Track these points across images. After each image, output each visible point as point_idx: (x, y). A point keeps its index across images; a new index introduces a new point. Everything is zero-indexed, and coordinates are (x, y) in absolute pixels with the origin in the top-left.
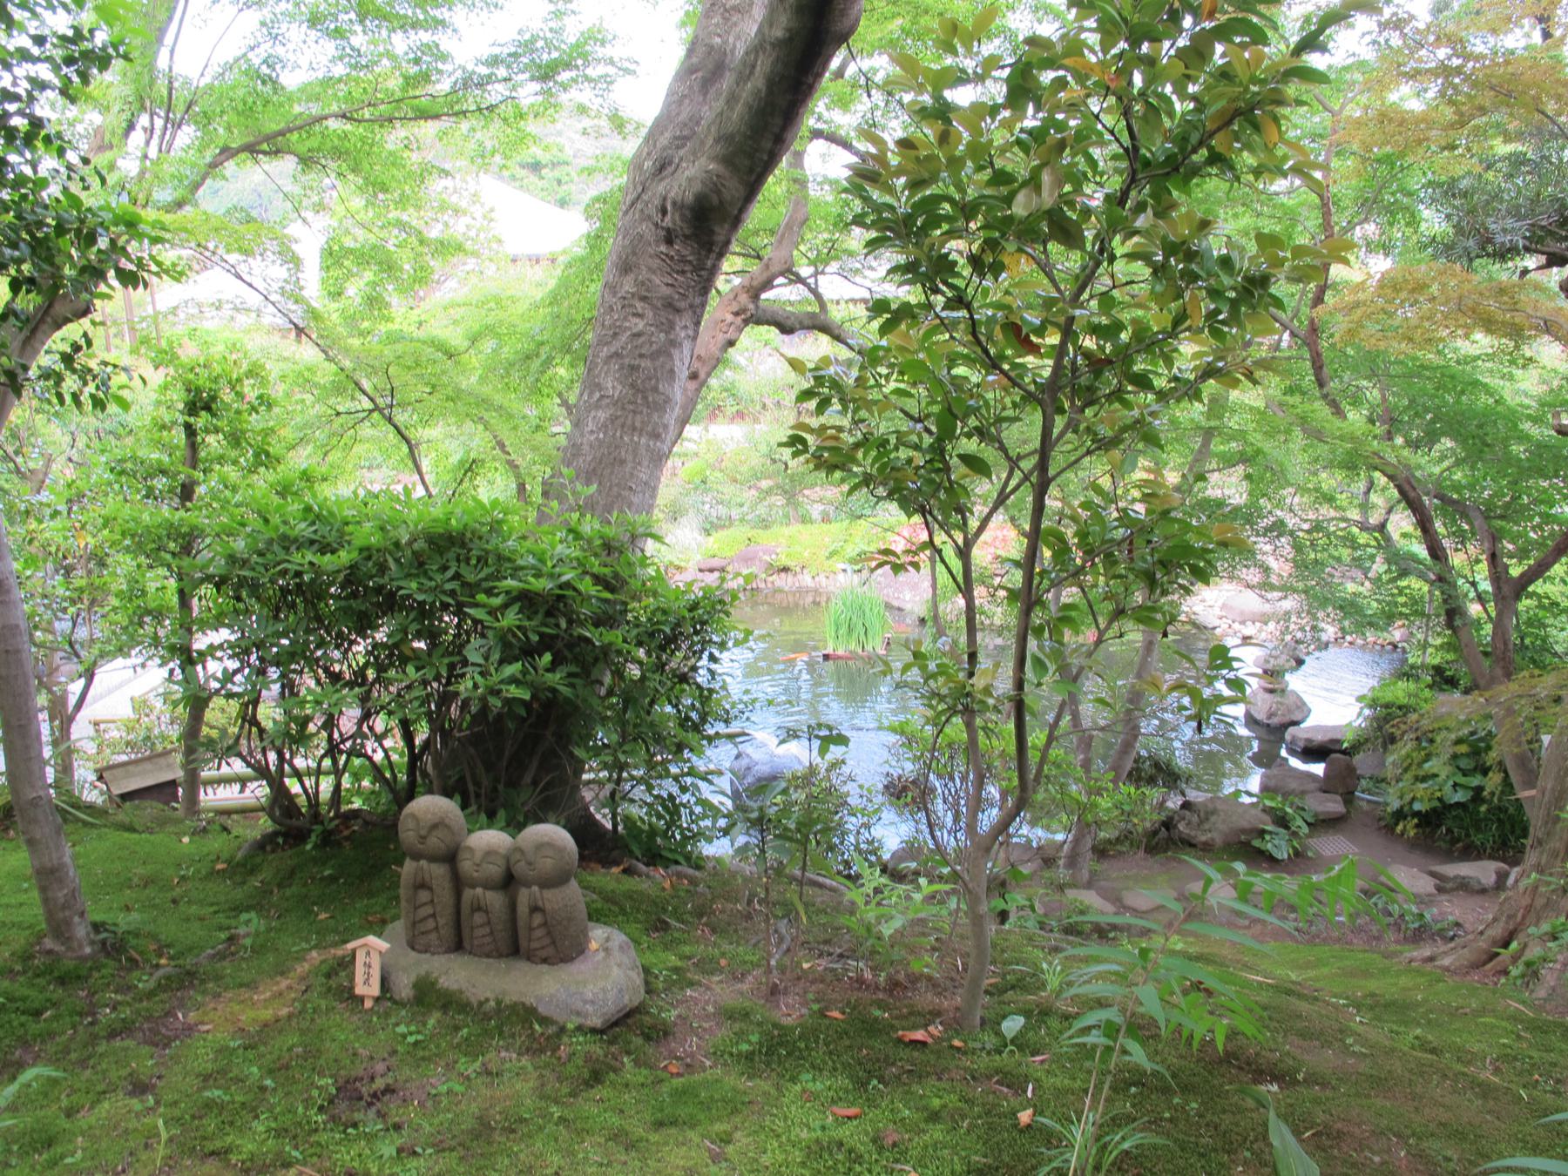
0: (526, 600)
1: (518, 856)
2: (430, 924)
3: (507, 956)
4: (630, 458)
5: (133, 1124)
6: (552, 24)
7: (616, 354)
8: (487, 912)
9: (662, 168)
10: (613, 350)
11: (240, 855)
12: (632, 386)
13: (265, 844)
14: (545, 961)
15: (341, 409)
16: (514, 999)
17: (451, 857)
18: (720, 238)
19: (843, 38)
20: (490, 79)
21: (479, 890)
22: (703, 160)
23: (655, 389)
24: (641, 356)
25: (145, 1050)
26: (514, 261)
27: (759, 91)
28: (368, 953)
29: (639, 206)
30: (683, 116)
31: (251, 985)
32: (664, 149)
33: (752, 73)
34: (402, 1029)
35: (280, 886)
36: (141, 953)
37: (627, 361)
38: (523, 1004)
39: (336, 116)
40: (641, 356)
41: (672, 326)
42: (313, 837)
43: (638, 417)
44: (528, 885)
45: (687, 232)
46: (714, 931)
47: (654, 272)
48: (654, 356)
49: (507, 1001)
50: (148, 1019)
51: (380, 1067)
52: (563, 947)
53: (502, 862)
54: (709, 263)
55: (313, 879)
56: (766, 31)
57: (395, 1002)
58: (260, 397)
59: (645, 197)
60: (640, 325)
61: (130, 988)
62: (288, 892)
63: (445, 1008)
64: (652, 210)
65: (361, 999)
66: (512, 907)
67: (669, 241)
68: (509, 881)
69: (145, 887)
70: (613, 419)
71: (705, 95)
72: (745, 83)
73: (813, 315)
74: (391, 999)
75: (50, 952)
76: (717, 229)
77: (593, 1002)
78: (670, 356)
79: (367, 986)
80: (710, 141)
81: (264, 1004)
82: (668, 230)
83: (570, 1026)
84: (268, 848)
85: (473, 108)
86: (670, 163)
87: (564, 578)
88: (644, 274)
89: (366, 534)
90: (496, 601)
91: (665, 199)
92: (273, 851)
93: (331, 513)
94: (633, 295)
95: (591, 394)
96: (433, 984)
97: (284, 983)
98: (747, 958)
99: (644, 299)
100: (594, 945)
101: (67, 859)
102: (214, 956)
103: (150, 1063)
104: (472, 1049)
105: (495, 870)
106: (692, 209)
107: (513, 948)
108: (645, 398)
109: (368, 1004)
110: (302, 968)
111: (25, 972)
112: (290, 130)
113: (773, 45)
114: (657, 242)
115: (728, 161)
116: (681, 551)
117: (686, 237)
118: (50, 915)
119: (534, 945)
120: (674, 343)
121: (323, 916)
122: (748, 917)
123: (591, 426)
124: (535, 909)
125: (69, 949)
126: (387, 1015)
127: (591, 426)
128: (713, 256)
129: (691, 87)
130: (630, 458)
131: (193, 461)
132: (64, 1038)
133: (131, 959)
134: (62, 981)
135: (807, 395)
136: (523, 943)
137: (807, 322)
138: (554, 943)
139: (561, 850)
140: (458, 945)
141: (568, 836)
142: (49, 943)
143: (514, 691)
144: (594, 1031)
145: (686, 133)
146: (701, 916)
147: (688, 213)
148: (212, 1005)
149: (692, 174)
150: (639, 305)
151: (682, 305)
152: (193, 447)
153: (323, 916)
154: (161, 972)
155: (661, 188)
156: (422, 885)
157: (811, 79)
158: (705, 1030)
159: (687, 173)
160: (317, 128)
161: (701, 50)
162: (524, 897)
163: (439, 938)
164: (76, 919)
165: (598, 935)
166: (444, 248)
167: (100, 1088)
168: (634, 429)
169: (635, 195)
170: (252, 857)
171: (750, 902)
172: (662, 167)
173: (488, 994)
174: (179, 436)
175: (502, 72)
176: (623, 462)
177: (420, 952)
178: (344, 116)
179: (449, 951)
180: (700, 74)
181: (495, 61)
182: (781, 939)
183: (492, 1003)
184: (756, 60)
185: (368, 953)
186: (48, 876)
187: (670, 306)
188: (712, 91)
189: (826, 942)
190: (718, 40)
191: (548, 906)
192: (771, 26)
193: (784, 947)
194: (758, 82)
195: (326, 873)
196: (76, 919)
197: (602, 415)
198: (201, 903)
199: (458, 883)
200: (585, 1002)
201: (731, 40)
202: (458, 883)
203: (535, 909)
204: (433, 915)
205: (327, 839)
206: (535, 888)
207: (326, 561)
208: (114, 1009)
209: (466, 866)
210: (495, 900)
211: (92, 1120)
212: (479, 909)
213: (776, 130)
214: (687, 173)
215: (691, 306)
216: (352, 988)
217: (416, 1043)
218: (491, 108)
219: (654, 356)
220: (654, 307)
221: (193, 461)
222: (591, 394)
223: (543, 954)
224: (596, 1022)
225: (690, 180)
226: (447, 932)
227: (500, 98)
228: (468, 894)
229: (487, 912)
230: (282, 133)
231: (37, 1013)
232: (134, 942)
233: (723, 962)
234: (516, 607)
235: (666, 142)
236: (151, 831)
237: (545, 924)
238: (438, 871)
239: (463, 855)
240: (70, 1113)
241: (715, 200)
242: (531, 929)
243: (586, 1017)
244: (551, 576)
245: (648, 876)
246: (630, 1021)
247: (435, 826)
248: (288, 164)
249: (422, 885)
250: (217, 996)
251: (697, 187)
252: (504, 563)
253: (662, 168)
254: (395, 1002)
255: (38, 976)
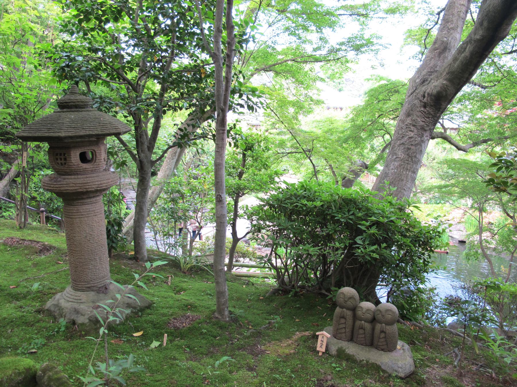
0: (377, 224)
1: (378, 312)
2: (343, 330)
3: (368, 346)
4: (405, 179)
5: (251, 381)
6: (360, 33)
7: (403, 143)
8: (364, 330)
9: (424, 82)
10: (402, 142)
11: (267, 295)
12: (408, 155)
13: (276, 292)
14: (382, 350)
15: (279, 152)
16: (373, 361)
17: (354, 309)
18: (443, 107)
19: (502, 39)
20: (338, 50)
21: (363, 322)
22: (441, 80)
23: (415, 157)
24: (412, 145)
25: (250, 356)
26: (329, 108)
27: (467, 57)
28: (323, 337)
29: (414, 94)
30: (431, 65)
31: (280, 340)
32: (424, 76)
33: (464, 51)
34: (334, 365)
35: (281, 307)
36: (243, 323)
37: (406, 146)
38: (376, 364)
39: (291, 60)
40: (412, 145)
41: (422, 135)
42: (291, 293)
43: (409, 166)
44: (381, 323)
45: (432, 104)
46: (431, 348)
47: (418, 117)
48: (416, 145)
49: (370, 361)
50: (249, 345)
51: (329, 377)
52: (389, 347)
53: (372, 313)
54: (438, 115)
55: (293, 307)
56: (473, 36)
57: (330, 355)
58: (266, 147)
59: (417, 91)
60: (412, 134)
61: (241, 334)
62: (285, 310)
63: (347, 360)
64: (419, 96)
65: (318, 352)
66: (373, 329)
67: (425, 107)
68: (374, 320)
69: (238, 301)
70: (400, 165)
71: (440, 57)
72: (461, 54)
73: (441, 133)
74: (328, 354)
75: (217, 318)
76: (443, 104)
77: (401, 368)
78: (421, 145)
79: (321, 348)
80: (445, 74)
81: (284, 347)
82: (425, 103)
83: (394, 375)
84: (276, 294)
85: (332, 59)
86: (427, 80)
87: (392, 219)
88: (415, 117)
89: (326, 197)
90: (368, 224)
91: (425, 92)
92: (278, 295)
93: (311, 188)
94: (410, 124)
95: (393, 156)
96: (344, 351)
97: (290, 342)
98: (445, 360)
99: (414, 126)
100: (398, 347)
101: (226, 290)
102: (265, 328)
103: (253, 361)
104: (359, 376)
105: (369, 316)
106: (435, 96)
107: (371, 343)
108: (412, 159)
109: (320, 354)
110: (295, 337)
111: (210, 323)
112: (277, 64)
113: (475, 41)
114: (420, 107)
115: (450, 80)
116: (424, 213)
117: (431, 106)
118: (218, 307)
119: (380, 344)
120: (423, 141)
121: (297, 320)
122: (443, 344)
123: (392, 167)
124: (382, 332)
125: (223, 318)
126: (327, 359)
127: (392, 167)
128: (440, 112)
129: (434, 55)
130: (405, 179)
131: (244, 165)
132: (224, 347)
133: (240, 324)
134: (221, 328)
135: (494, 165)
136: (375, 342)
137: (439, 136)
138: (387, 344)
139: (394, 313)
140: (351, 339)
141: (395, 307)
142: (216, 315)
143: (375, 255)
144: (401, 378)
145: (432, 70)
146: (425, 341)
147: (433, 97)
148: (268, 345)
149: (435, 85)
150: (412, 128)
151: (427, 128)
152: (244, 161)
153: (297, 320)
154: (251, 331)
155: (423, 89)
156: (343, 317)
157: (487, 53)
158: (437, 385)
159: (434, 84)
160: (284, 63)
161: (439, 43)
162: (378, 327)
163: (346, 336)
164: (226, 309)
165: (400, 344)
166: (318, 102)
167: (239, 366)
168: (407, 169)
169: (413, 90)
170: (272, 296)
171: (442, 339)
172: (423, 81)
173: (363, 358)
174: (240, 157)
175: (344, 47)
176: (402, 180)
177: (338, 339)
178: (293, 60)
179: (348, 341)
180: (438, 51)
181: (342, 44)
182: (457, 355)
183: (365, 362)
184: (467, 46)
185: (323, 337)
186: (220, 294)
187: (423, 129)
188: (442, 56)
189: (475, 359)
190: (445, 39)
191: (387, 332)
192: (475, 34)
193: (459, 358)
194: (467, 53)
195: (297, 306)
196: (226, 309)
197: (396, 164)
198: (257, 309)
199: (355, 317)
200: (399, 367)
201: (450, 39)
202: (355, 317)
203: (382, 332)
204: (345, 328)
205: (296, 294)
206: (384, 325)
207: (310, 204)
208: (238, 340)
209: (359, 313)
210: (368, 326)
211: (238, 376)
212: (362, 328)
213: (471, 71)
214: (434, 84)
215: (430, 129)
216: (316, 347)
217: (339, 371)
218: (338, 59)
219: (416, 145)
220: (417, 129)
221: (244, 165)
222: (393, 156)
223: (383, 347)
224: (402, 375)
225: (435, 86)
226: (349, 334)
227: (341, 56)
228: (358, 323)
229: (364, 330)
230: (274, 65)
231: (215, 337)
232: (240, 319)
233: (437, 360)
234: (375, 227)
235: (425, 73)
236: (231, 281)
237: (385, 337)
238: (349, 313)
239: (358, 309)
240: (231, 372)
241: (444, 93)
242: (379, 338)
243: (398, 373)
244: (387, 217)
245: (404, 324)
246: (412, 377)
247: (350, 298)
248: (272, 74)
249: (343, 317)
250: (269, 342)
251: (438, 89)
252: (369, 213)
253: (424, 82)
254: (330, 355)
255: (214, 325)
